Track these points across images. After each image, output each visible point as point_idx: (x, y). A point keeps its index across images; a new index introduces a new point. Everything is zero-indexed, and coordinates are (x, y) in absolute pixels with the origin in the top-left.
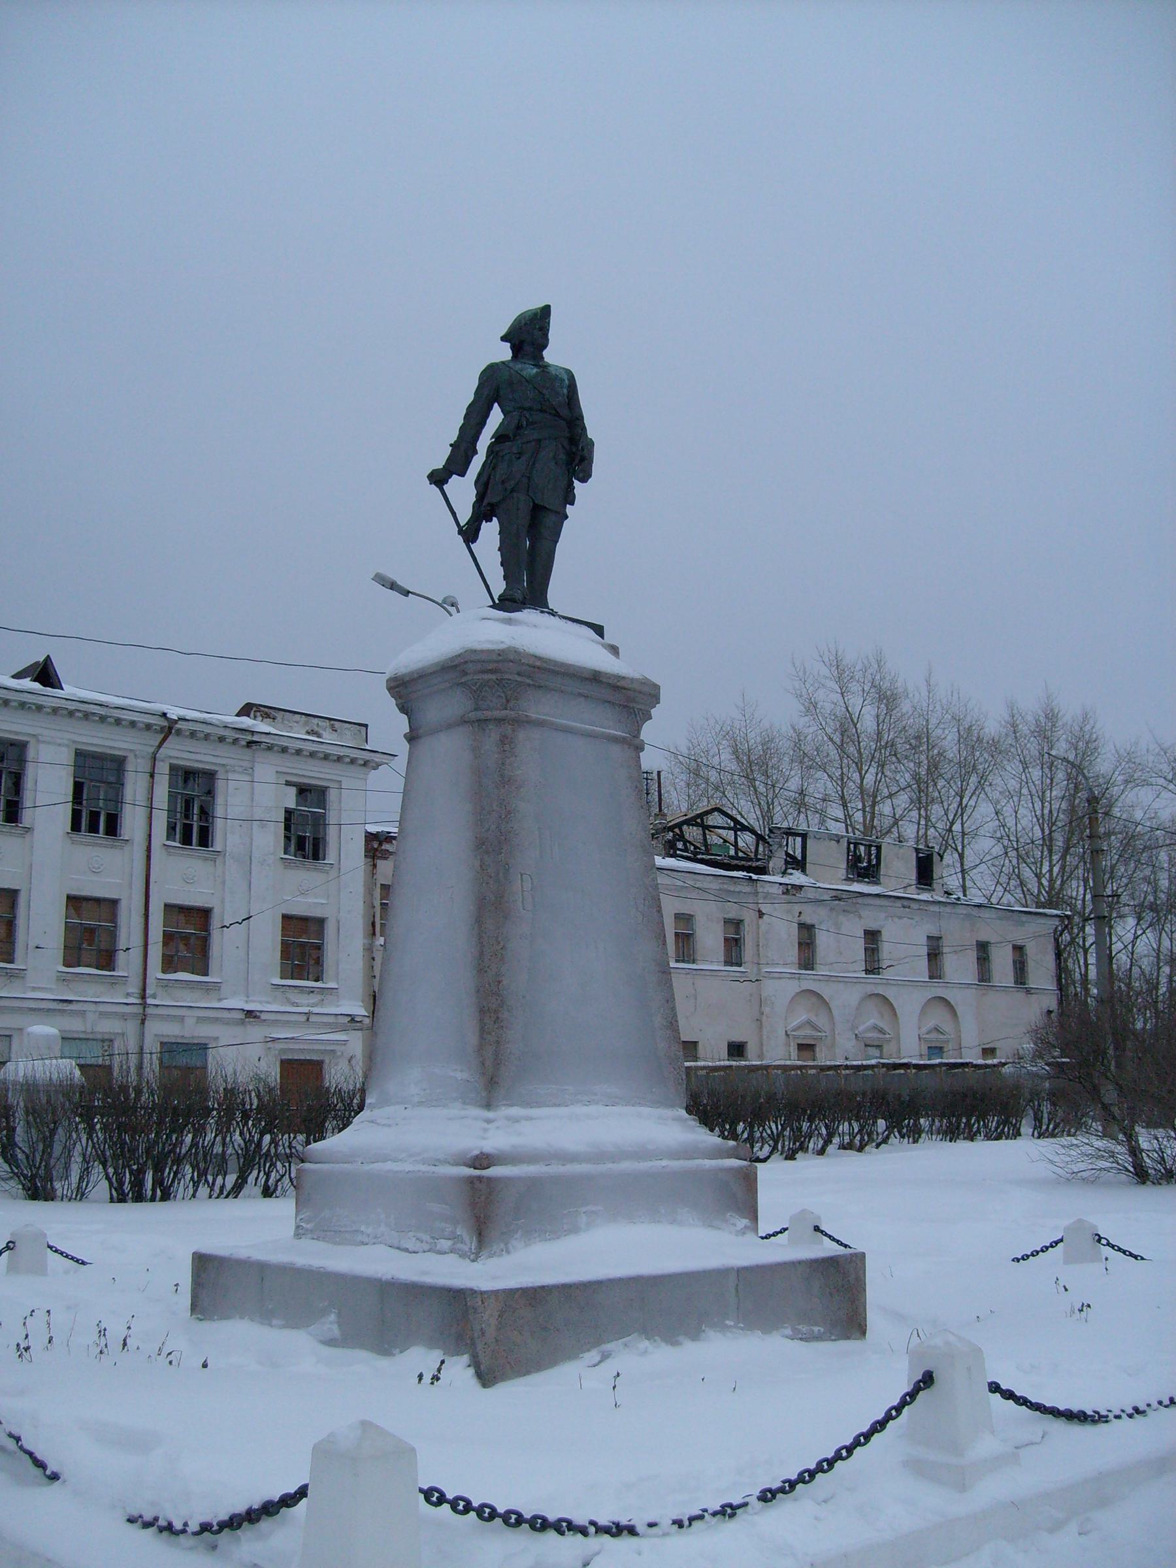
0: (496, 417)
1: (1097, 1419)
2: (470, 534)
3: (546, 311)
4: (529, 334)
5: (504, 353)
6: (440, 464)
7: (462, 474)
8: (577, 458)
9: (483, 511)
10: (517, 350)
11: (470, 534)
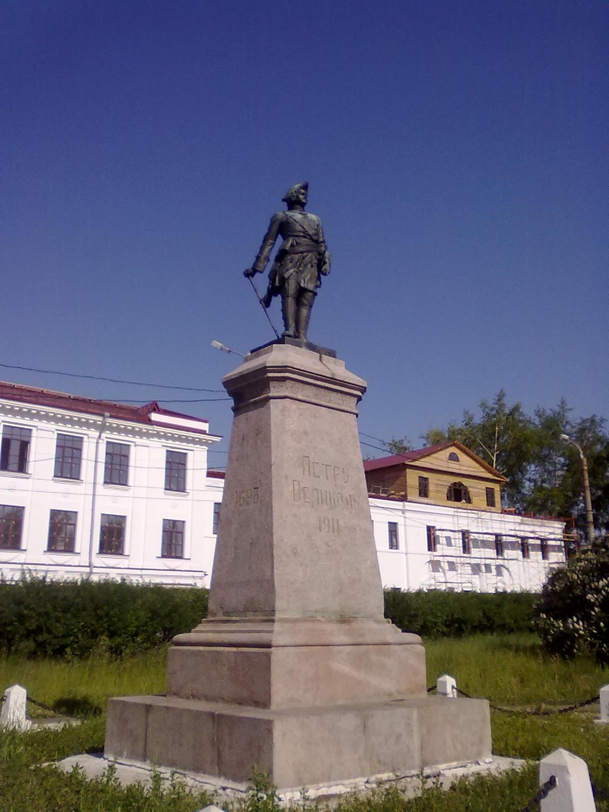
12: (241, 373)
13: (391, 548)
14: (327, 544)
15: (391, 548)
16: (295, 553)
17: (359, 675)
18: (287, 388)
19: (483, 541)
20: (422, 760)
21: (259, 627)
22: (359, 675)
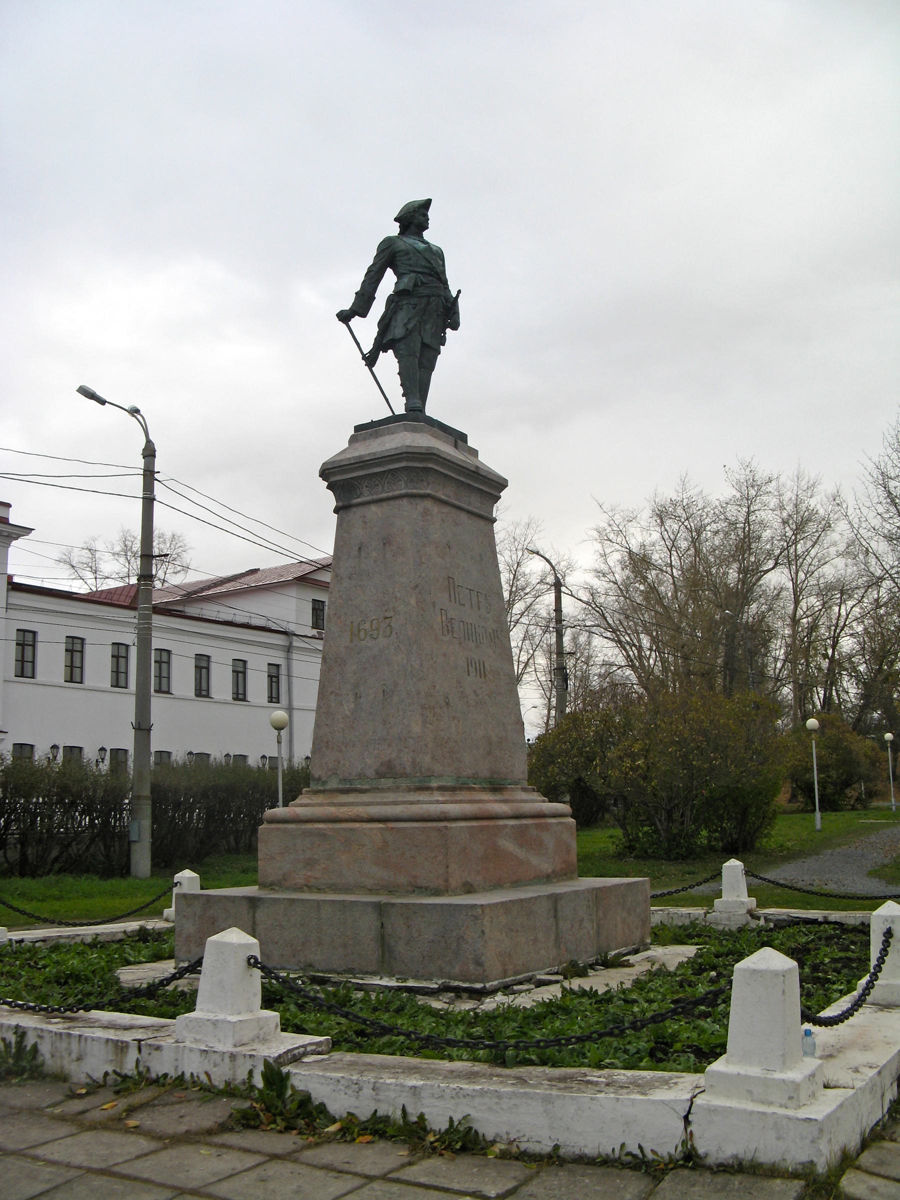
0: (389, 282)
1: (103, 402)
2: (370, 360)
3: (428, 203)
4: (414, 218)
5: (394, 230)
6: (347, 305)
7: (364, 315)
8: (447, 313)
9: (381, 345)
10: (404, 230)
11: (370, 360)
12: (360, 457)
13: (270, 701)
14: (475, 692)
15: (270, 701)
16: (448, 704)
17: (520, 853)
18: (428, 484)
19: (452, 1072)
20: (619, 856)
21: (412, 797)
22: (520, 853)
